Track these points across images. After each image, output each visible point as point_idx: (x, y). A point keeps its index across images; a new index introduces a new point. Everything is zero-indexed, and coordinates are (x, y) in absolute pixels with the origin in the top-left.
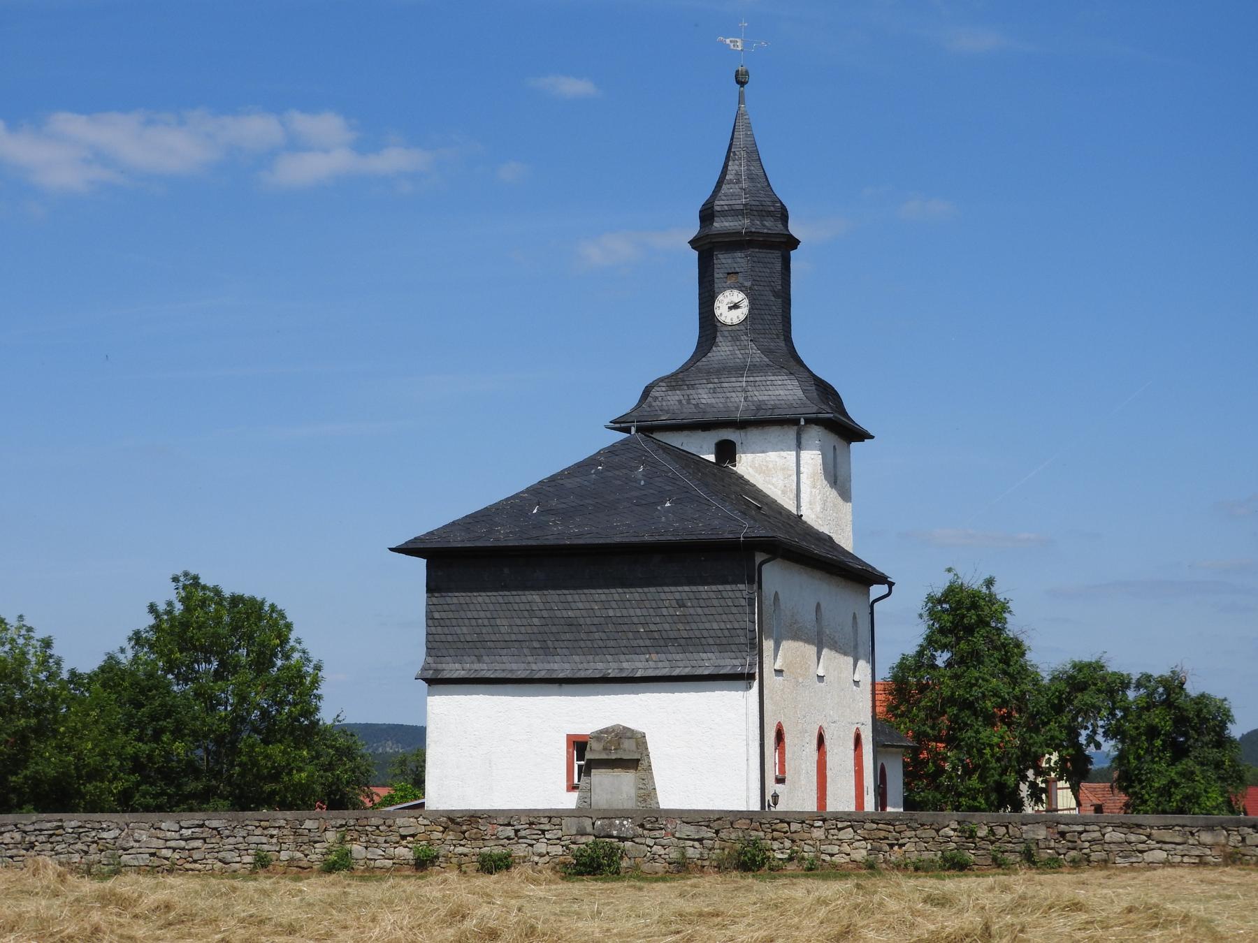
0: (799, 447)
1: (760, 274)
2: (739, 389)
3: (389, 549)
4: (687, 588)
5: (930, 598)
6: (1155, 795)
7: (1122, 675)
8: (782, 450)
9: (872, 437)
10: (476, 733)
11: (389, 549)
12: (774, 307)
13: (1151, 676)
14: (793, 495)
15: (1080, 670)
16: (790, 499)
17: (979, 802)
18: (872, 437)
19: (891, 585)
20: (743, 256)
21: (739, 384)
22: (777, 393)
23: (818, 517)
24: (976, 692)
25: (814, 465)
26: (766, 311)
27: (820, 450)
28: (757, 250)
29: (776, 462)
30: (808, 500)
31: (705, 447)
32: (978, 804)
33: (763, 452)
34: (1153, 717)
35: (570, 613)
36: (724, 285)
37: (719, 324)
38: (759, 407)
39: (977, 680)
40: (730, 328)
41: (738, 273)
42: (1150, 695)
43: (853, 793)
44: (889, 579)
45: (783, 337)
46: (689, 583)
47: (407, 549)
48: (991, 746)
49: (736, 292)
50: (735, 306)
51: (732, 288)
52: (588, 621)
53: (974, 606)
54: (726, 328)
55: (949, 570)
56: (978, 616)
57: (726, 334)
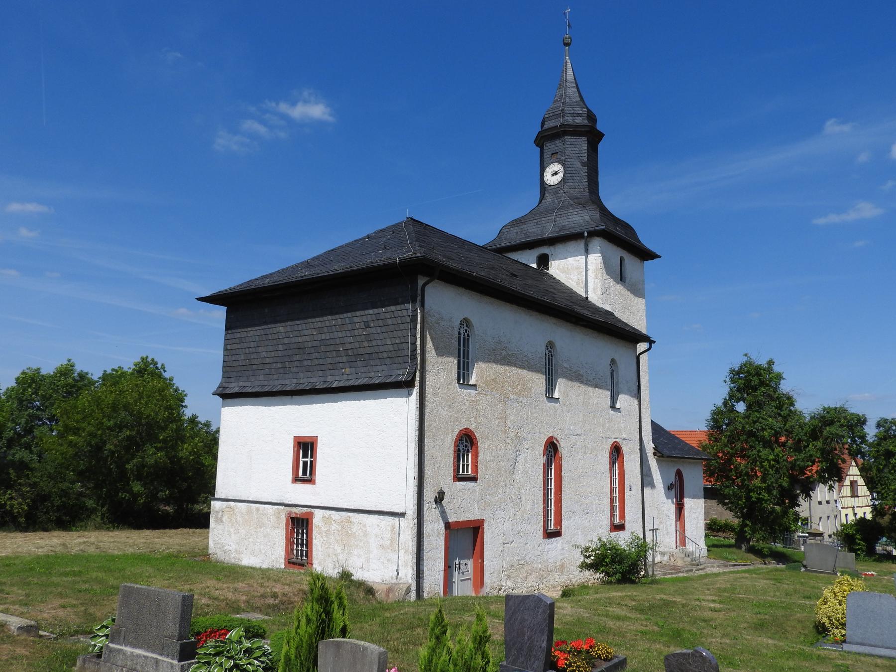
0: (587, 252)
1: (571, 152)
2: (551, 221)
3: (197, 299)
4: (371, 311)
5: (732, 371)
6: (892, 494)
7: (858, 415)
8: (577, 256)
9: (659, 257)
10: (245, 436)
11: (197, 299)
12: (582, 172)
13: (887, 420)
14: (583, 285)
15: (828, 412)
16: (581, 288)
17: (763, 495)
18: (659, 257)
19: (651, 342)
20: (560, 141)
21: (551, 218)
22: (574, 219)
23: (599, 298)
24: (758, 425)
25: (597, 264)
26: (576, 175)
27: (600, 253)
28: (570, 137)
29: (573, 264)
30: (592, 287)
31: (531, 260)
32: (762, 497)
33: (565, 259)
34: (888, 444)
35: (300, 339)
36: (550, 162)
37: (546, 186)
38: (563, 228)
39: (758, 418)
40: (553, 187)
41: (557, 153)
42: (886, 431)
43: (312, 505)
44: (651, 339)
45: (588, 190)
46: (373, 307)
47: (214, 299)
48: (769, 461)
49: (556, 164)
50: (556, 173)
51: (554, 162)
52: (310, 344)
53: (758, 374)
54: (550, 188)
55: (746, 355)
56: (760, 380)
57: (550, 191)
